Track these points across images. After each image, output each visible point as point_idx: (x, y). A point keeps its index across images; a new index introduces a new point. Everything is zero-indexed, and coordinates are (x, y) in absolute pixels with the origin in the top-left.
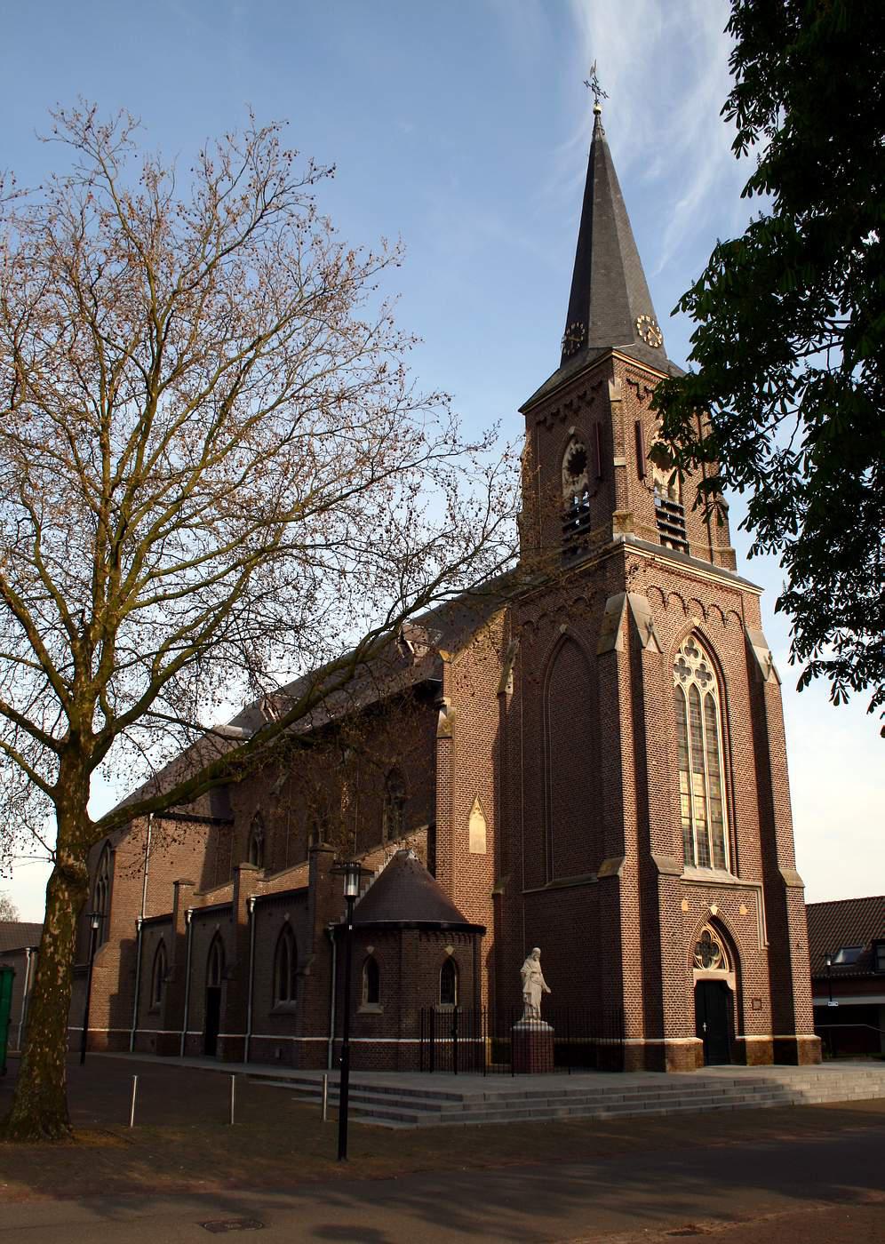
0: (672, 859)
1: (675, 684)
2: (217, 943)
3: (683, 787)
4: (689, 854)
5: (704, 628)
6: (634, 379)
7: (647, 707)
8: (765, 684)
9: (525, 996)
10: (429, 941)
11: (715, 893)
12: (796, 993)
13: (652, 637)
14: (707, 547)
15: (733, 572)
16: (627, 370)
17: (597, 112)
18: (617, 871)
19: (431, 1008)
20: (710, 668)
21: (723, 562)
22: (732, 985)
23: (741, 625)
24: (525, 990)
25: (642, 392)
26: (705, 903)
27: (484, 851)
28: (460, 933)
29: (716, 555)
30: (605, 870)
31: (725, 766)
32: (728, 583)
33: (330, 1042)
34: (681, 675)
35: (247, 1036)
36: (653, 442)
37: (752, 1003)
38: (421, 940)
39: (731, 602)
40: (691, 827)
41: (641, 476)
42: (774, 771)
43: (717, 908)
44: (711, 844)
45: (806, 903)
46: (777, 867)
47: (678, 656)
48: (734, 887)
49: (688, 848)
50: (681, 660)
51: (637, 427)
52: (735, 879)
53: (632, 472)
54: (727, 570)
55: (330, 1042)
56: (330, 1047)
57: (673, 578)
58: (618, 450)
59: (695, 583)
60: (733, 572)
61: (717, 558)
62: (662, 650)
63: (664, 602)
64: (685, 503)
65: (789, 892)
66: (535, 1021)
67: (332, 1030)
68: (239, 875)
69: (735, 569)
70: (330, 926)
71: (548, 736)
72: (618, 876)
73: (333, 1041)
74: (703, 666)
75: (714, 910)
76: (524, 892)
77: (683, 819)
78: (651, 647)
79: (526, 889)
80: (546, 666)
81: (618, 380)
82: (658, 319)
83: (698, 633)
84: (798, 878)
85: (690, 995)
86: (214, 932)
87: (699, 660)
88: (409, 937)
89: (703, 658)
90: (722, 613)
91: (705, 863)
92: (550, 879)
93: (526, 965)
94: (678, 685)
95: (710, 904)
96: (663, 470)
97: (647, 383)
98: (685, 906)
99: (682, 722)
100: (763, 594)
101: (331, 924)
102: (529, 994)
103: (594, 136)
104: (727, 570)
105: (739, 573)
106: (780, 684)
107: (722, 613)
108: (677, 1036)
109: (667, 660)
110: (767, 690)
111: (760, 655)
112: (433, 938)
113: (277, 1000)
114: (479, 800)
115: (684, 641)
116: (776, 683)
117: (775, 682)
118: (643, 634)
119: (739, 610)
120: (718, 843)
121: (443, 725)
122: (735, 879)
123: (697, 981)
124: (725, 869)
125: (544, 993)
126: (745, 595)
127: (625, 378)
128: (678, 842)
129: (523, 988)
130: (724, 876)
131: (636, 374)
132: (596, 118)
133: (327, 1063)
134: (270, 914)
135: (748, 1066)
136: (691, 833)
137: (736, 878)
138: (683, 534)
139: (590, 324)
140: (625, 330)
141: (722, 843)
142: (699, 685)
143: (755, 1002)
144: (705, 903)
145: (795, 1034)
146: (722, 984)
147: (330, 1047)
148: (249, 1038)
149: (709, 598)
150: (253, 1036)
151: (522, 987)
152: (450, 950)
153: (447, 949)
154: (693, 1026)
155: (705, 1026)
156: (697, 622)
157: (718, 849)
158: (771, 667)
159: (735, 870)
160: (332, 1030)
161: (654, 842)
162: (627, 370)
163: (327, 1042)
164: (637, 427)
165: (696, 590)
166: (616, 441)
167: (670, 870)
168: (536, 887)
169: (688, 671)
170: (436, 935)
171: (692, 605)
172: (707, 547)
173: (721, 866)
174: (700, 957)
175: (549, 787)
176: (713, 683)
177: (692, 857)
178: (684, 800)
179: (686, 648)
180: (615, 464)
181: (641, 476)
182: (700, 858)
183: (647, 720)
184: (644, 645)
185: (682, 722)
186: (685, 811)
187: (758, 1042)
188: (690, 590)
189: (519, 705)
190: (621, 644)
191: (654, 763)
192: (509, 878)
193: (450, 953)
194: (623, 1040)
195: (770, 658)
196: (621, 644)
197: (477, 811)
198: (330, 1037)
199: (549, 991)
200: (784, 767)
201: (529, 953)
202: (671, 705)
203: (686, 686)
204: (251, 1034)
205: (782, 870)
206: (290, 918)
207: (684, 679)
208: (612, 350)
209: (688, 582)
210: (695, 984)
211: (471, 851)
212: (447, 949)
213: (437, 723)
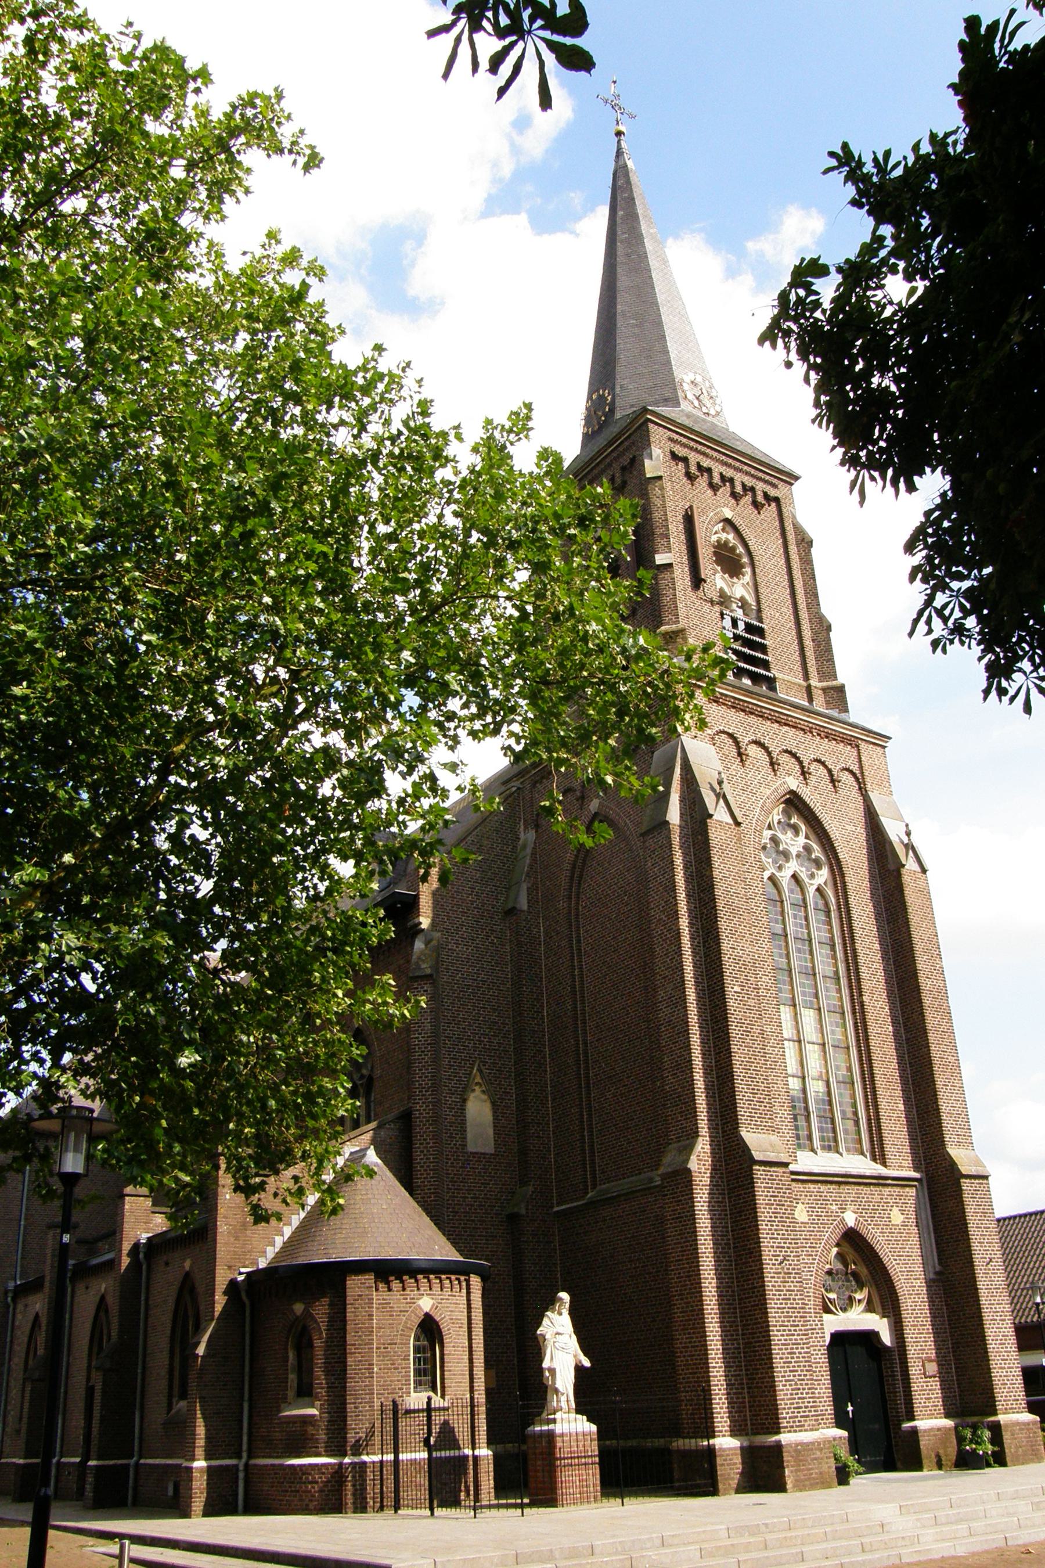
0: (774, 1138)
1: (767, 874)
2: (102, 1314)
3: (788, 1031)
4: (803, 1133)
5: (807, 794)
6: (681, 452)
7: (720, 904)
8: (903, 871)
9: (547, 1374)
10: (390, 1290)
11: (850, 1192)
12: (992, 1345)
13: (721, 801)
14: (805, 684)
15: (843, 716)
16: (671, 439)
17: (619, 134)
18: (687, 1160)
19: (394, 1402)
20: (817, 852)
21: (828, 703)
22: (886, 1339)
23: (860, 789)
24: (546, 1364)
25: (693, 469)
26: (834, 1207)
27: (490, 1149)
28: (453, 1277)
29: (818, 695)
30: (669, 1160)
31: (852, 996)
32: (837, 728)
33: (241, 1468)
34: (775, 862)
35: (132, 1461)
36: (714, 538)
37: (923, 1366)
38: (377, 1290)
39: (840, 756)
40: (804, 1090)
41: (697, 581)
42: (927, 1001)
43: (854, 1216)
44: (838, 1116)
45: (999, 1213)
46: (942, 1144)
47: (768, 834)
48: (879, 1181)
49: (802, 1122)
50: (774, 840)
51: (689, 520)
52: (879, 1169)
53: (681, 575)
54: (834, 713)
55: (241, 1468)
56: (241, 1475)
57: (752, 719)
58: (660, 542)
59: (786, 728)
60: (843, 716)
61: (818, 695)
62: (740, 820)
63: (740, 754)
64: (766, 620)
65: (966, 1185)
66: (565, 1416)
67: (245, 1447)
68: (123, 1204)
69: (846, 710)
70: (240, 1273)
71: (581, 968)
72: (689, 1171)
73: (246, 1465)
74: (807, 849)
75: (850, 1219)
76: (556, 1209)
77: (790, 1079)
78: (720, 814)
79: (558, 1204)
80: (574, 867)
81: (656, 451)
82: (713, 381)
83: (794, 803)
84: (978, 1163)
85: (821, 1360)
86: (97, 1299)
87: (801, 840)
88: (357, 1285)
89: (807, 837)
90: (830, 771)
91: (832, 1146)
92: (594, 1186)
93: (546, 1321)
94: (770, 878)
95: (843, 1210)
96: (731, 577)
97: (700, 458)
98: (801, 1214)
99: (780, 932)
100: (889, 744)
101: (243, 1270)
102: (552, 1371)
103: (616, 162)
104: (834, 713)
105: (853, 717)
106: (924, 871)
107: (830, 771)
108: (801, 1428)
109: (750, 838)
110: (906, 879)
111: (894, 831)
112: (396, 1285)
113: (174, 1400)
114: (480, 1070)
115: (775, 811)
116: (918, 869)
117: (916, 867)
118: (709, 799)
119: (855, 768)
120: (850, 1115)
121: (419, 958)
122: (879, 1169)
123: (832, 1335)
124: (862, 1154)
125: (579, 1369)
126: (863, 745)
127: (667, 450)
128: (783, 1113)
129: (542, 1361)
130: (863, 1165)
131: (685, 446)
132: (619, 142)
133: (237, 1505)
134: (167, 1264)
135: (925, 1473)
136: (805, 1100)
137: (879, 1167)
138: (766, 665)
139: (618, 390)
140: (668, 395)
141: (856, 1113)
142: (804, 876)
143: (927, 1364)
144: (834, 1207)
145: (778, 1433)
146: (869, 1337)
147: (241, 1475)
148: (137, 1464)
149: (811, 748)
150: (142, 1461)
151: (540, 1356)
152: (426, 1304)
153: (421, 1302)
154: (830, 1410)
155: (850, 1408)
156: (793, 783)
157: (850, 1124)
158: (909, 847)
159: (879, 1155)
160: (245, 1447)
161: (743, 1111)
162: (671, 439)
163: (236, 1466)
164: (689, 520)
165: (790, 738)
166: (658, 531)
167: (772, 1157)
168: (572, 1200)
169: (786, 855)
170: (402, 1282)
171: (785, 758)
172: (805, 684)
173: (856, 1150)
174: (832, 1296)
175: (585, 1043)
176: (823, 875)
177: (810, 1137)
178: (790, 1051)
179: (779, 822)
180: (658, 562)
181: (697, 581)
182: (822, 1139)
183: (722, 924)
184: (711, 812)
185: (780, 932)
186: (792, 1066)
187: (939, 1429)
188: (780, 738)
189: (538, 926)
190: (674, 814)
191: (737, 989)
192: (531, 1188)
193: (427, 1309)
194: (711, 1441)
195: (908, 834)
196: (674, 814)
197: (477, 1088)
198: (240, 1457)
199: (586, 1363)
200: (943, 993)
201: (550, 1302)
202: (759, 905)
203: (784, 877)
204: (141, 1457)
205: (953, 1151)
206: (191, 1267)
207: (780, 868)
208: (645, 410)
209: (776, 725)
210: (828, 1339)
211: (471, 1148)
212: (421, 1302)
213: (411, 955)
